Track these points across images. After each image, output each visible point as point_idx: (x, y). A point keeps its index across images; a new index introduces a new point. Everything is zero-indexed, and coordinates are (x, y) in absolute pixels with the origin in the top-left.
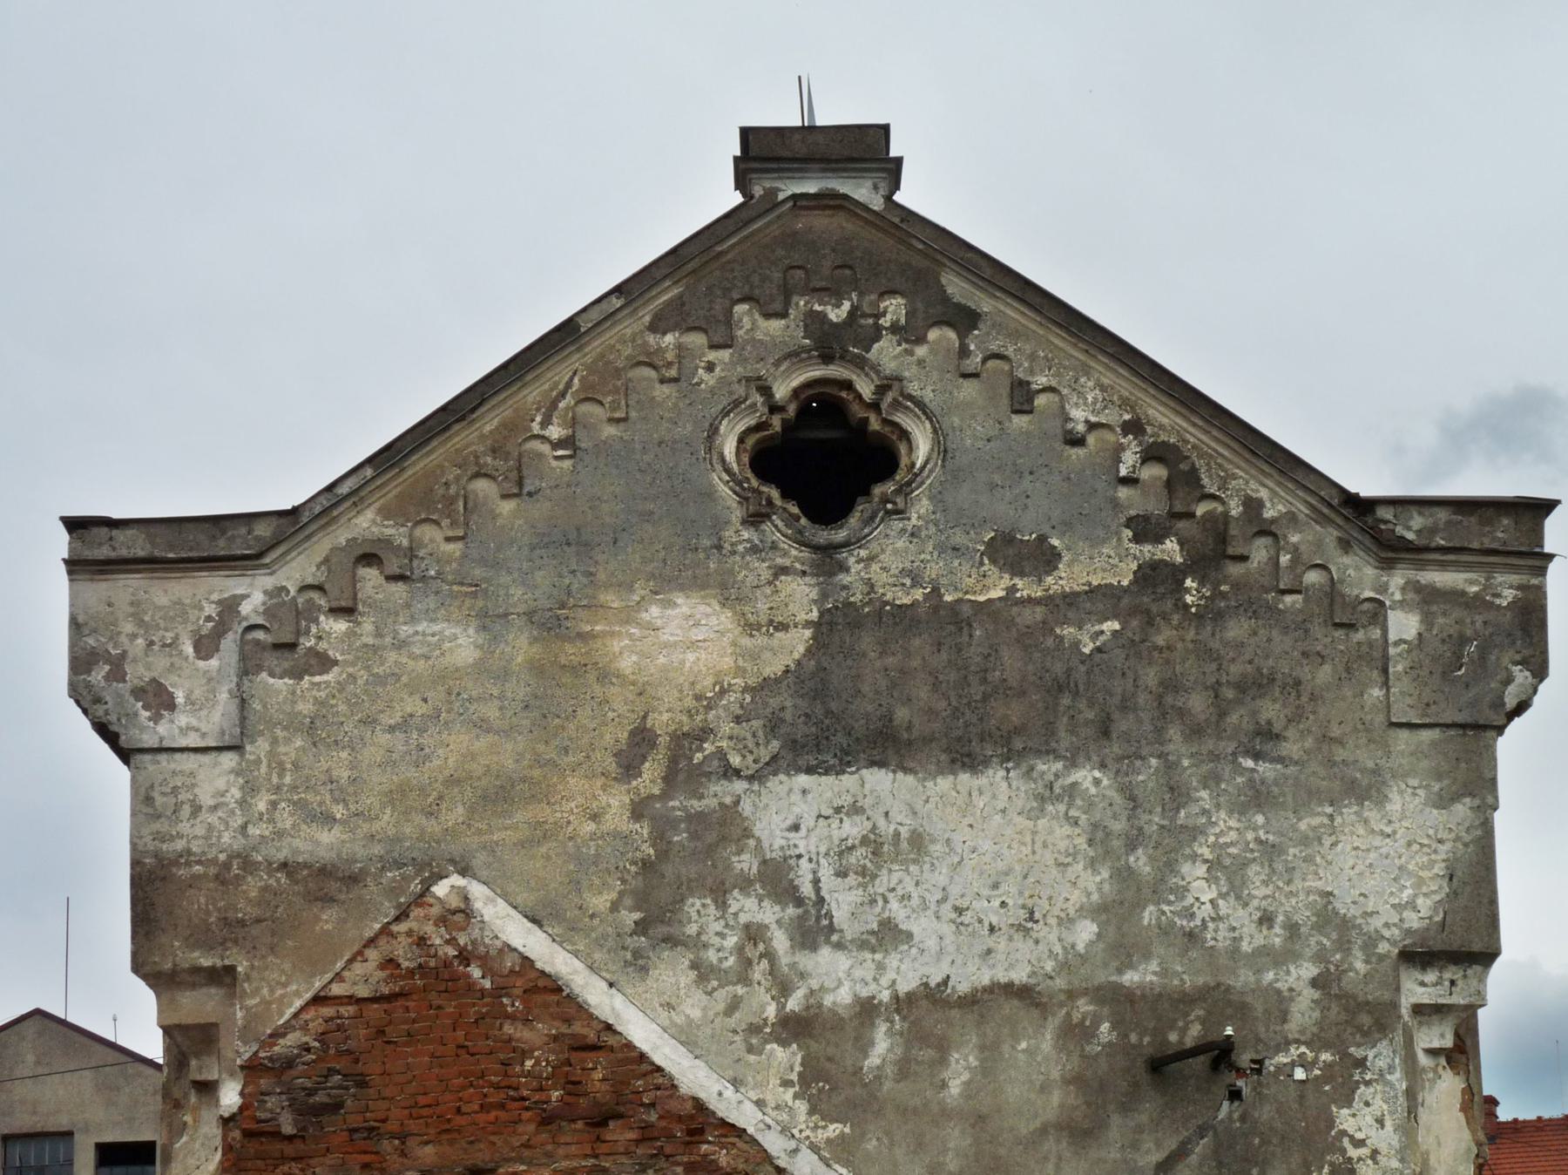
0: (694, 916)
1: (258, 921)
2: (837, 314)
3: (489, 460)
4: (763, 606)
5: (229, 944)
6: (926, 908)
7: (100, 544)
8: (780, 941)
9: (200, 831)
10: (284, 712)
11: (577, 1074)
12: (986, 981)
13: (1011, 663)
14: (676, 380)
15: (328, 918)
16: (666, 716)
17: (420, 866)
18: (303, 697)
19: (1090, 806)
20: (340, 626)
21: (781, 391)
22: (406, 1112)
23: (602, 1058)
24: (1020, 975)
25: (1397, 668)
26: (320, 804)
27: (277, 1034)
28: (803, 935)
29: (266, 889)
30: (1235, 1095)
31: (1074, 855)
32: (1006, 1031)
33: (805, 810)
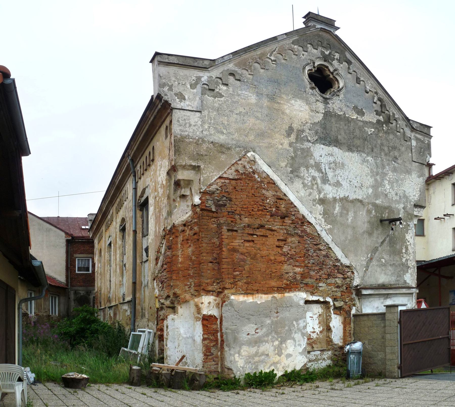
0: (302, 172)
1: (206, 155)
2: (327, 53)
3: (259, 60)
4: (314, 107)
6: (345, 180)
7: (166, 59)
8: (319, 181)
9: (191, 131)
10: (211, 105)
12: (355, 198)
13: (357, 132)
14: (297, 55)
15: (223, 157)
16: (296, 125)
17: (244, 148)
18: (216, 103)
19: (370, 165)
20: (225, 88)
21: (316, 64)
22: (241, 209)
24: (360, 198)
25: (413, 151)
28: (323, 180)
30: (392, 229)
31: (368, 174)
32: (358, 209)
33: (323, 153)
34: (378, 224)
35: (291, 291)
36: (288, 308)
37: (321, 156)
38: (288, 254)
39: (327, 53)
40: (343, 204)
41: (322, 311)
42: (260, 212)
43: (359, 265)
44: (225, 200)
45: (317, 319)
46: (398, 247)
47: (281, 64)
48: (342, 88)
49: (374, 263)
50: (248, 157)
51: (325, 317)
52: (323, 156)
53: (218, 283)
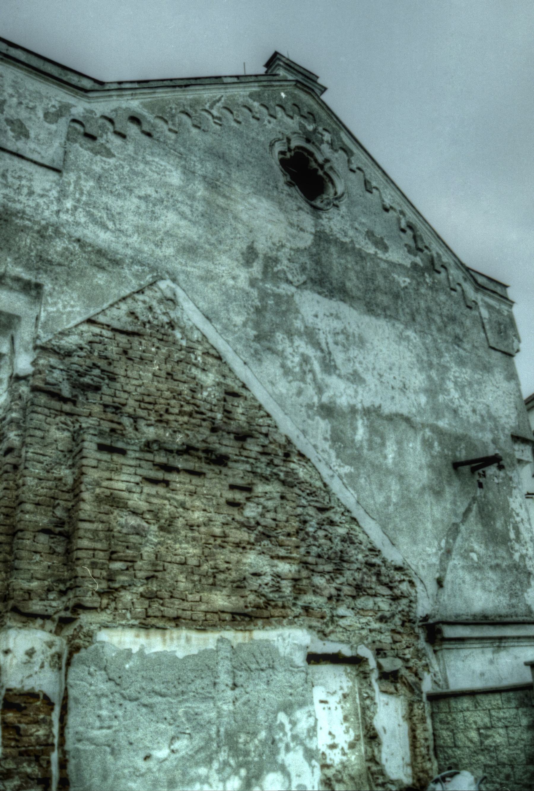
1: (60, 265)
2: (310, 128)
5: (41, 271)
8: (317, 367)
9: (32, 204)
11: (229, 407)
15: (101, 278)
17: (153, 269)
19: (415, 347)
20: (117, 141)
22: (138, 403)
23: (241, 402)
24: (405, 411)
25: (487, 327)
26: (101, 217)
27: (63, 334)
29: (67, 249)
34: (450, 473)
35: (270, 624)
36: (263, 674)
37: (316, 316)
38: (258, 524)
39: (310, 128)
40: (372, 423)
41: (350, 684)
42: (186, 419)
43: (424, 564)
44: (99, 377)
45: (339, 706)
46: (499, 525)
47: (230, 128)
48: (343, 195)
49: (456, 561)
50: (160, 289)
51: (358, 701)
52: (321, 315)
53: (62, 593)
